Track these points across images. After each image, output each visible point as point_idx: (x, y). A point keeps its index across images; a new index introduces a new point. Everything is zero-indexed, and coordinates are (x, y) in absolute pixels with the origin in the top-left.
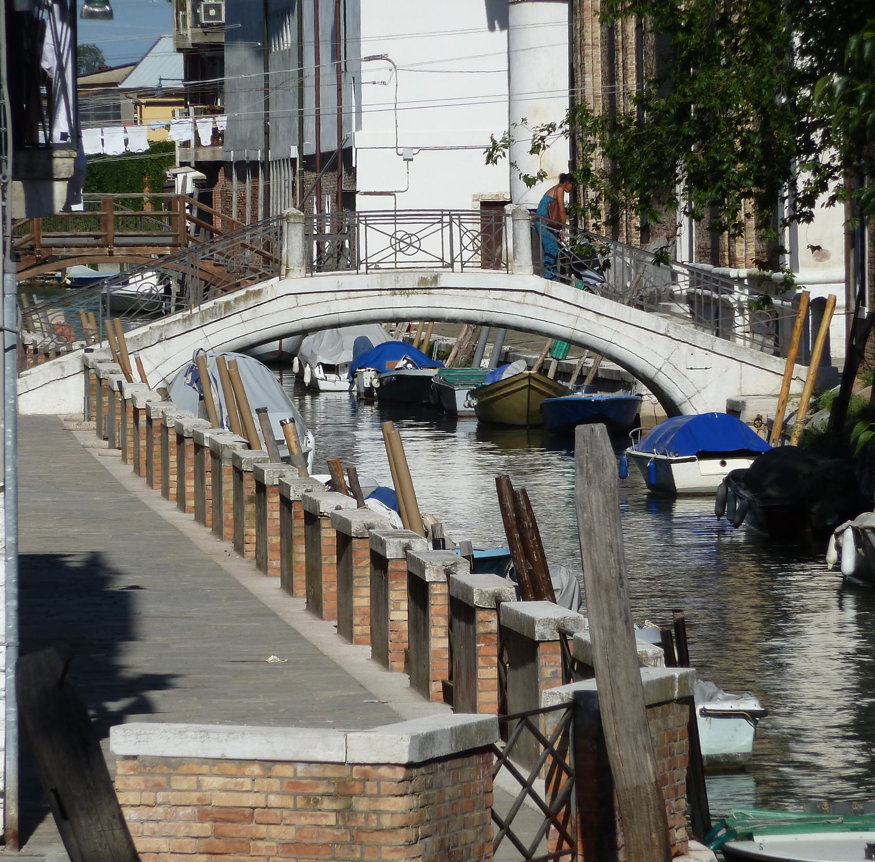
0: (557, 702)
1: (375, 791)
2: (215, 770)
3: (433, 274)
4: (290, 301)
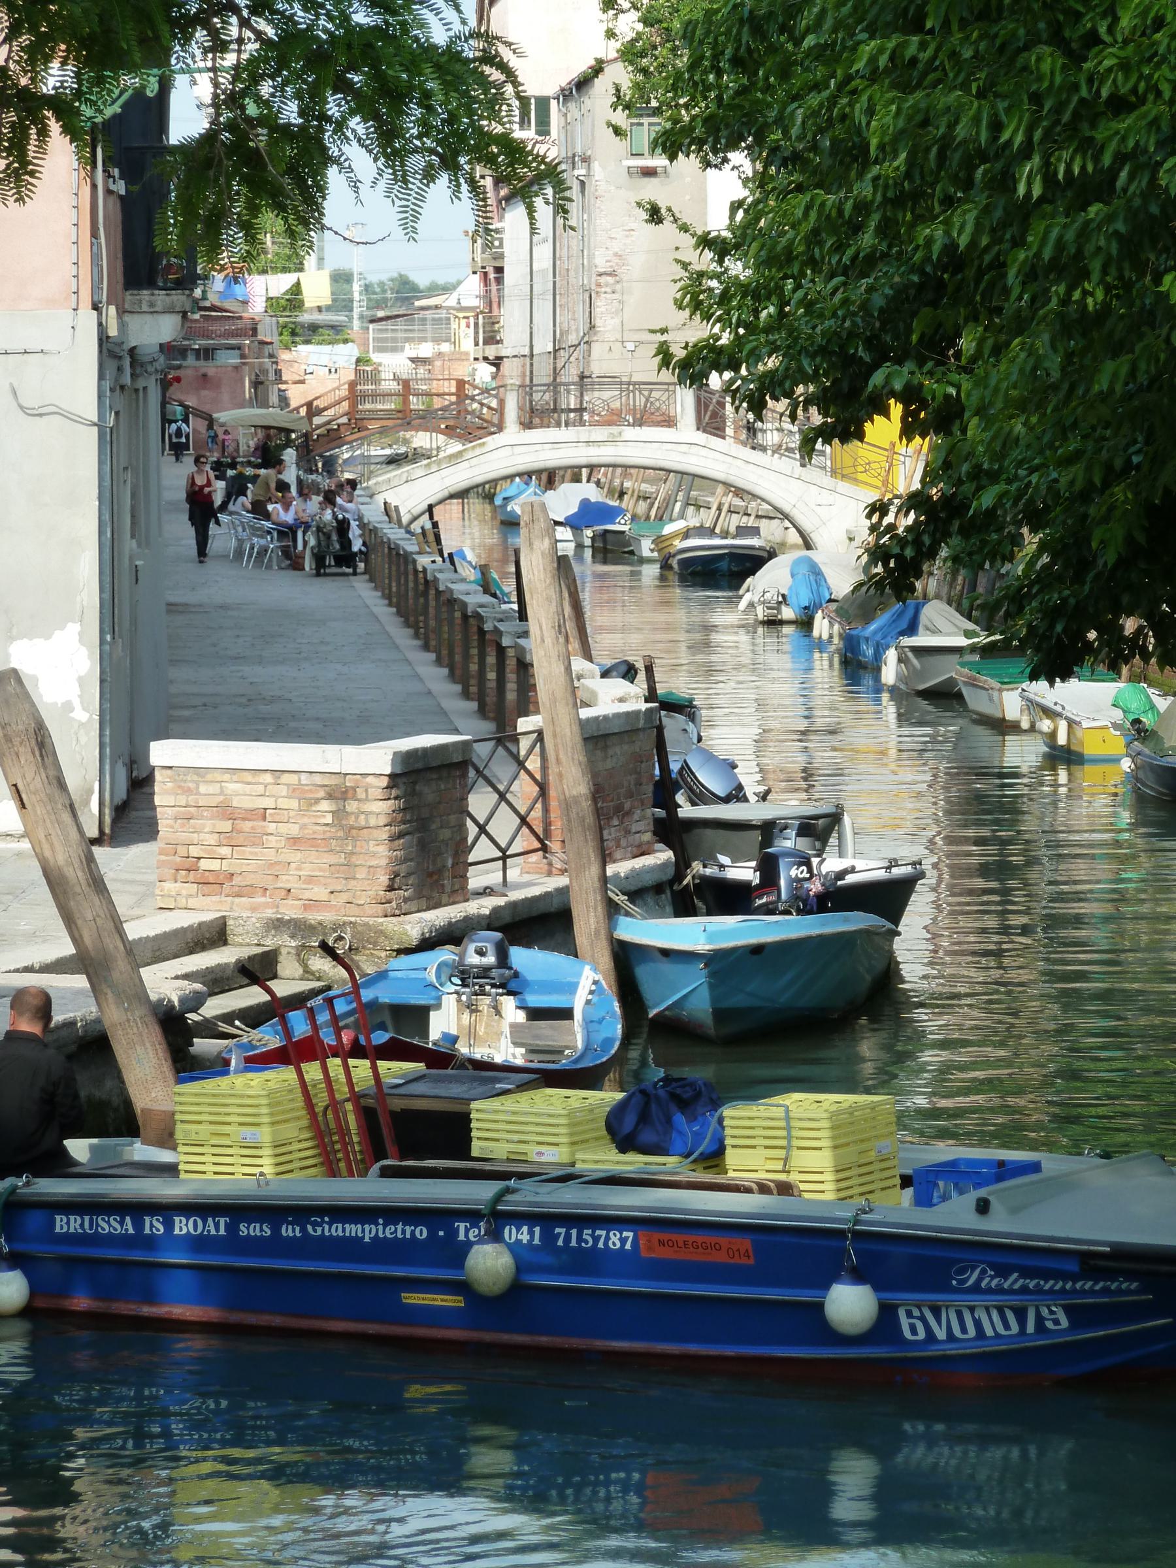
2: (235, 778)
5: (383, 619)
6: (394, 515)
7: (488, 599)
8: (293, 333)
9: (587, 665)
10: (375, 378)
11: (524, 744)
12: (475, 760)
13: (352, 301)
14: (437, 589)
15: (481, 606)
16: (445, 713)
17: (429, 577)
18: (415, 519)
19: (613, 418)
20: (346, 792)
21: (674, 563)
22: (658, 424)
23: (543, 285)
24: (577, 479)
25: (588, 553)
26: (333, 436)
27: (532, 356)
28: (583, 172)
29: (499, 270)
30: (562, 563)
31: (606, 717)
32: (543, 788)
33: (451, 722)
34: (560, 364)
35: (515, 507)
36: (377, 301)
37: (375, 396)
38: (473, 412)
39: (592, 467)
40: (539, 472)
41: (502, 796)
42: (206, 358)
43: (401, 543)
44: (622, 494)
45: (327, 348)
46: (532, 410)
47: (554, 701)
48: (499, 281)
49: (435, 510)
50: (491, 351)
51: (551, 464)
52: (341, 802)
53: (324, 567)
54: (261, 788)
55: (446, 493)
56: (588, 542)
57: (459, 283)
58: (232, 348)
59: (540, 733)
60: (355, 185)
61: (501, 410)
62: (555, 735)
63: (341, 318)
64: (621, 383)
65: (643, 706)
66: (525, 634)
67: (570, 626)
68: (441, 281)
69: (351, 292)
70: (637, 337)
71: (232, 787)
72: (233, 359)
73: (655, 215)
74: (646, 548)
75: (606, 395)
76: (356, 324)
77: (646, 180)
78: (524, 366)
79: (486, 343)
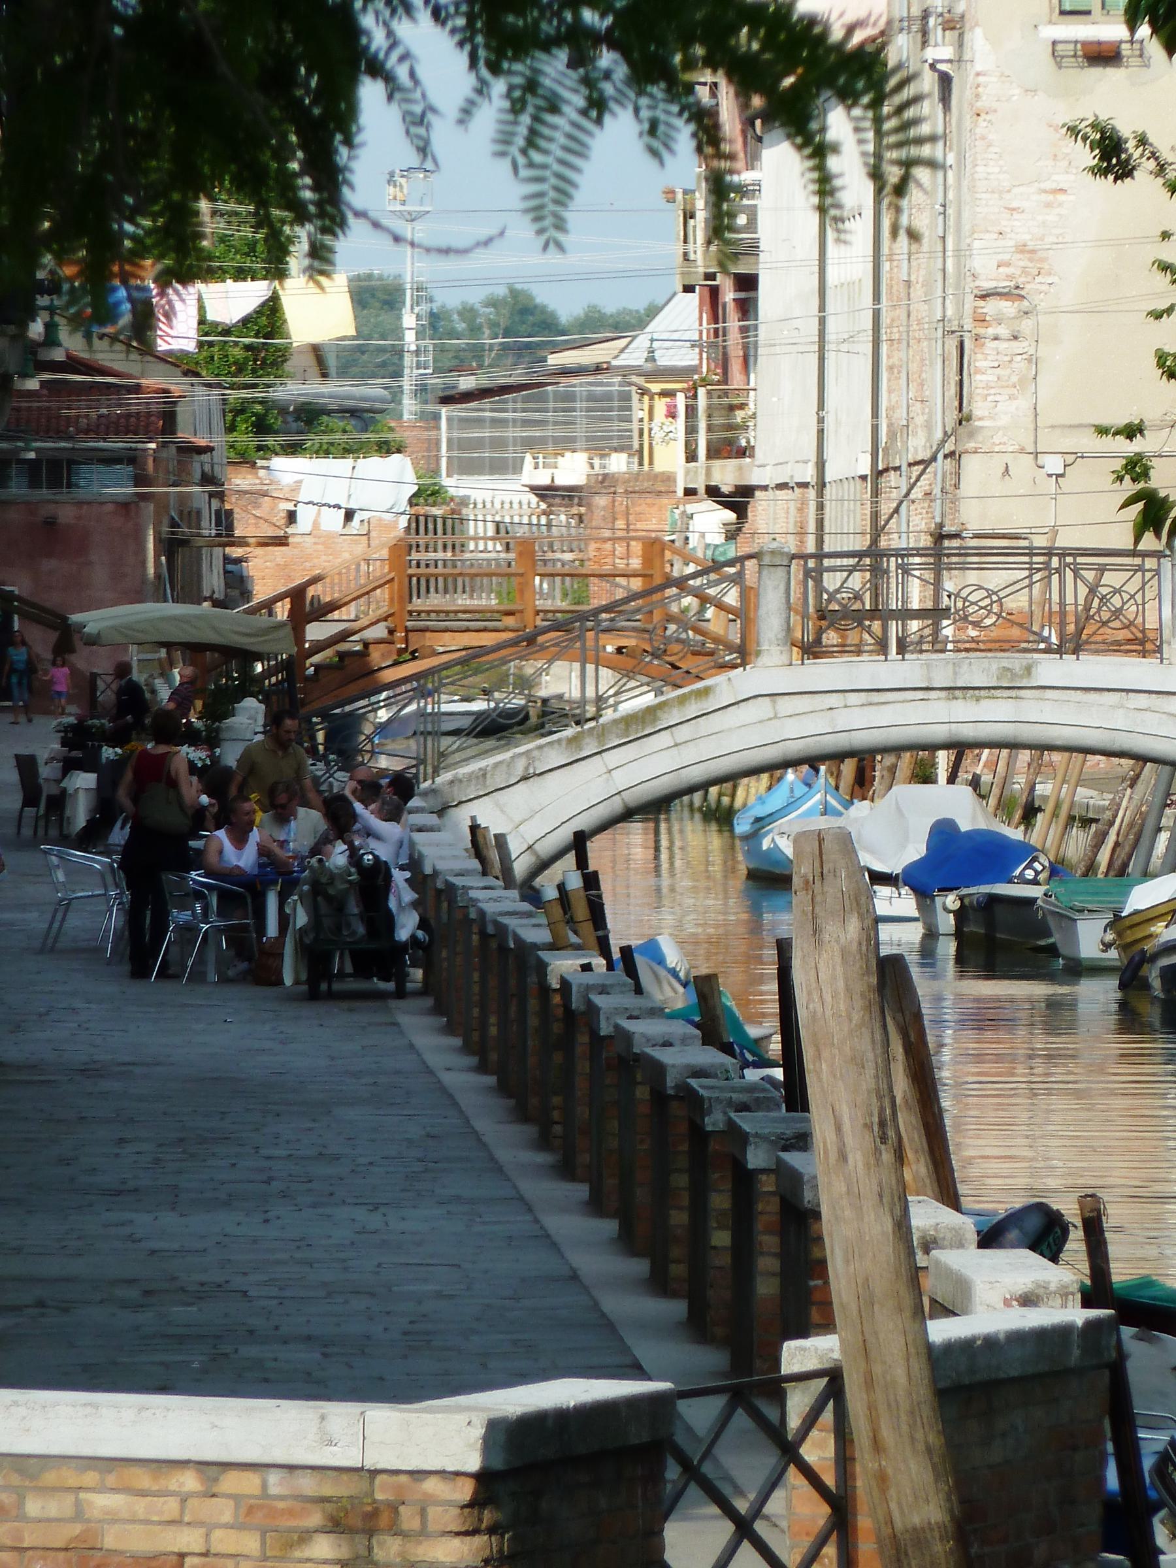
0: (811, 1365)
1: (415, 1524)
2: (111, 1480)
3: (1024, 662)
4: (762, 708)
5: (467, 1101)
6: (494, 855)
7: (711, 1057)
8: (261, 427)
9: (946, 1216)
10: (454, 522)
11: (798, 1403)
12: (680, 1439)
13: (399, 352)
14: (594, 1033)
15: (699, 1073)
16: (608, 1326)
17: (576, 1003)
18: (543, 865)
19: (1015, 637)
20: (374, 1514)
21: (1154, 976)
22: (1116, 648)
23: (850, 320)
24: (924, 776)
25: (948, 948)
26: (353, 671)
27: (822, 485)
28: (946, 52)
29: (747, 283)
30: (890, 980)
31: (990, 1343)
32: (841, 1507)
33: (626, 1350)
34: (886, 508)
35: (780, 841)
36: (458, 352)
37: (450, 582)
38: (680, 619)
39: (960, 748)
40: (838, 757)
41: (744, 1529)
42: (55, 483)
43: (511, 922)
44: (1030, 812)
45: (342, 466)
46: (822, 614)
47: (867, 1301)
48: (747, 308)
49: (592, 846)
50: (726, 474)
51: (862, 739)
52: (361, 1540)
53: (329, 976)
54: (171, 1507)
55: (616, 806)
56: (947, 923)
57: (653, 311)
58: (111, 459)
59: (834, 1378)
60: (417, 122)
61: (744, 614)
62: (869, 1383)
63: (371, 390)
64: (1031, 552)
65: (1078, 1315)
66: (802, 1141)
67: (908, 1123)
68: (610, 307)
69: (397, 332)
70: (1071, 442)
71: (102, 1502)
72: (118, 487)
73: (1112, 155)
74: (1090, 938)
75: (995, 579)
76: (409, 406)
77: (1097, 72)
78: (804, 502)
79: (714, 452)
